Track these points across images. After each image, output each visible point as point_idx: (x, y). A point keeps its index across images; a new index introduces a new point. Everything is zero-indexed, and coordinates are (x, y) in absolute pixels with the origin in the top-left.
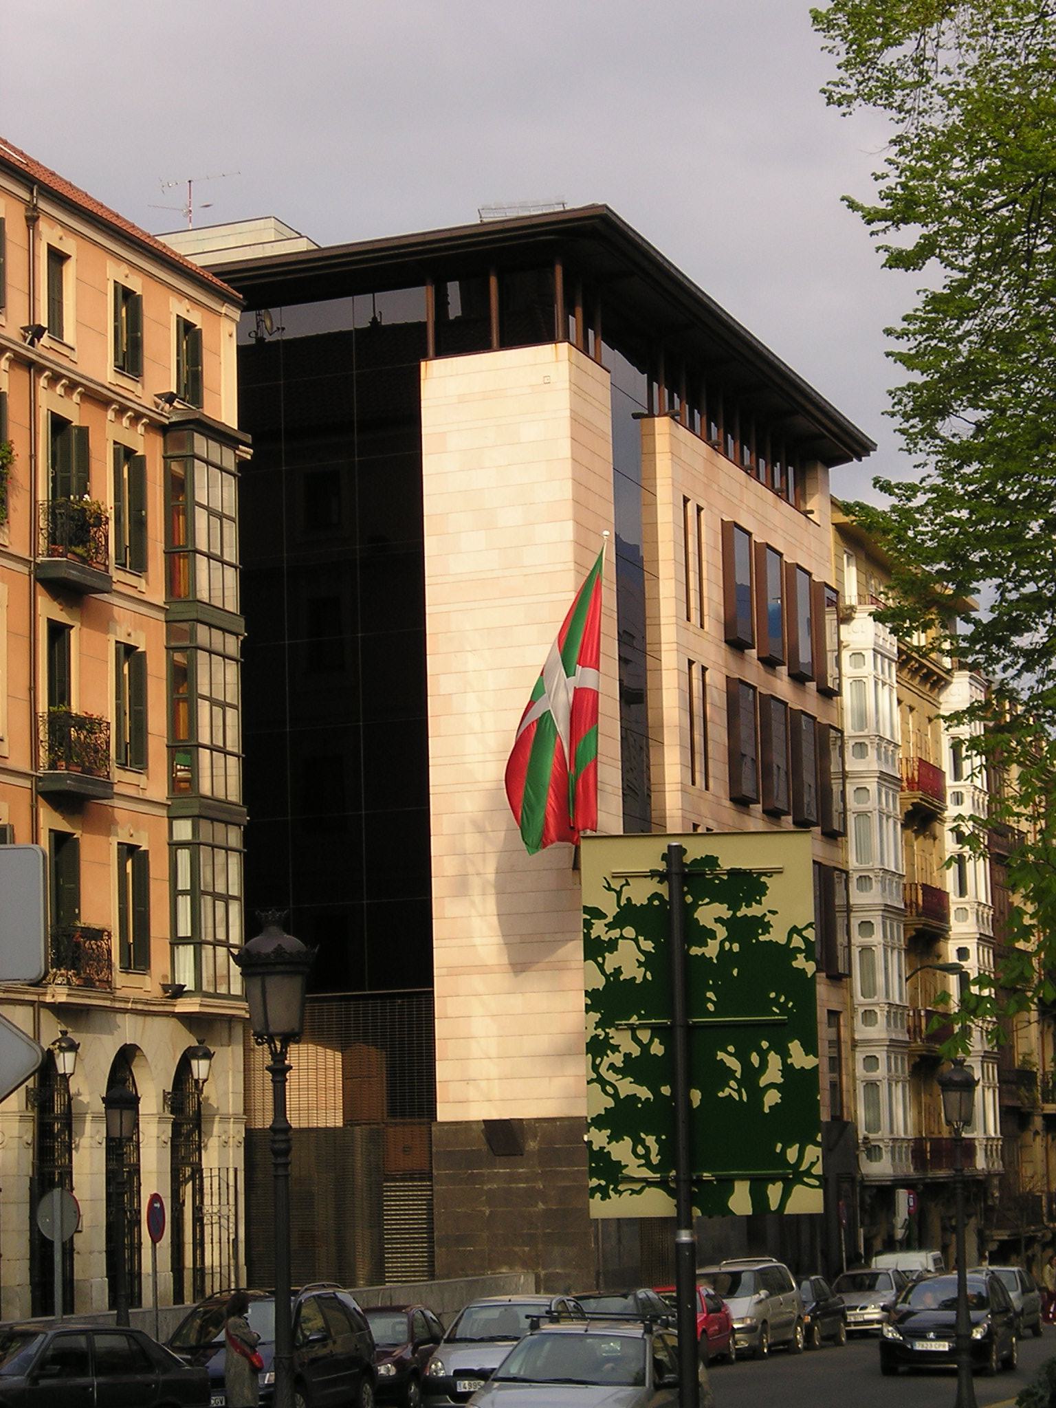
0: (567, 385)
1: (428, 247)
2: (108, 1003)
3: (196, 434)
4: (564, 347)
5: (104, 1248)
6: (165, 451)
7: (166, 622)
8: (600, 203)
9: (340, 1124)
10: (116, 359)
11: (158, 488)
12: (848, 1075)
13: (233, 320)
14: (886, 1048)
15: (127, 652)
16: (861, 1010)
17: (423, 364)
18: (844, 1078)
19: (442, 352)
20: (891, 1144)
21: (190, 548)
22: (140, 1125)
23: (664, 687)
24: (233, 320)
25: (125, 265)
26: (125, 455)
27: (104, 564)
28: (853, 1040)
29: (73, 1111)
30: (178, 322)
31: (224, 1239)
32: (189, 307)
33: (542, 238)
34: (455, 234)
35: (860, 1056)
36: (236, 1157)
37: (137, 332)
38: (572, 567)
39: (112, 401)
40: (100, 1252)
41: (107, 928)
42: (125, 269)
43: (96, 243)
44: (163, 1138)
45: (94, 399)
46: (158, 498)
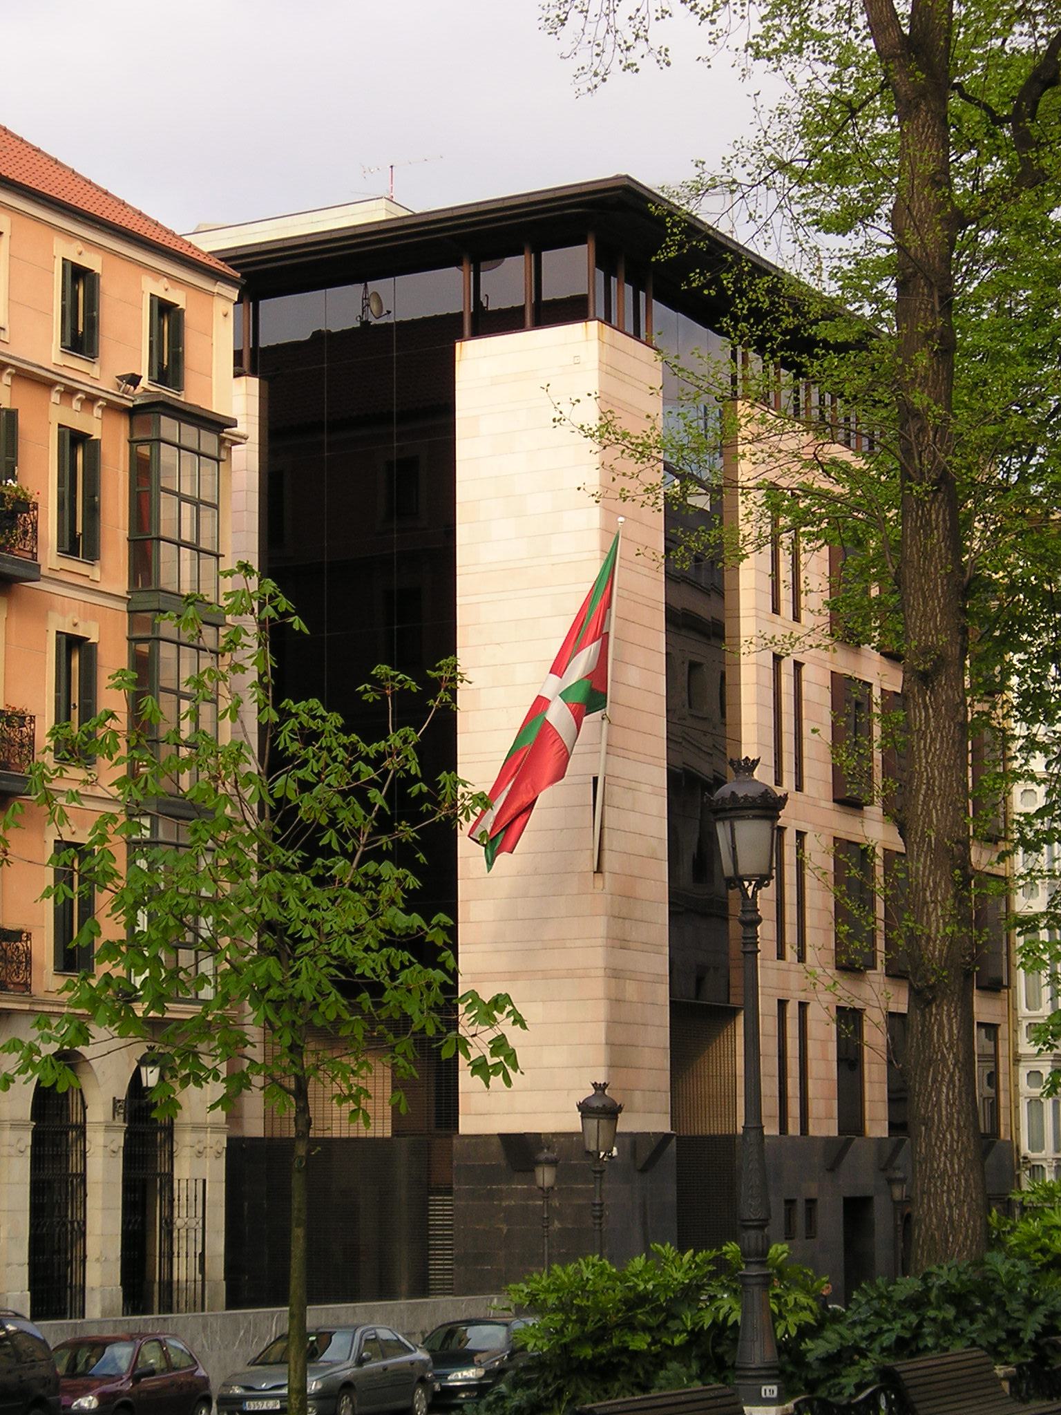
0: (596, 364)
1: (456, 222)
2: (27, 1007)
3: (162, 417)
4: (594, 325)
5: (27, 1260)
6: (131, 434)
7: (129, 612)
8: (624, 174)
9: (388, 1134)
10: (63, 340)
11: (121, 472)
12: (1005, 1091)
13: (229, 300)
14: (1050, 1063)
15: (72, 644)
16: (1025, 1024)
17: (458, 345)
18: (1002, 1094)
19: (477, 333)
20: (1054, 1164)
21: (154, 535)
22: (87, 1134)
23: (742, 682)
24: (229, 300)
25: (79, 243)
26: (74, 440)
27: (31, 552)
28: (1016, 1053)
29: (88, 1120)
30: (151, 301)
31: (191, 1254)
32: (167, 286)
33: (569, 211)
34: (482, 208)
35: (1023, 1072)
36: (215, 1171)
37: (93, 311)
38: (598, 556)
39: (55, 383)
40: (21, 1265)
41: (24, 928)
42: (78, 245)
43: (38, 220)
44: (114, 1147)
45: (25, 378)
46: (121, 483)
